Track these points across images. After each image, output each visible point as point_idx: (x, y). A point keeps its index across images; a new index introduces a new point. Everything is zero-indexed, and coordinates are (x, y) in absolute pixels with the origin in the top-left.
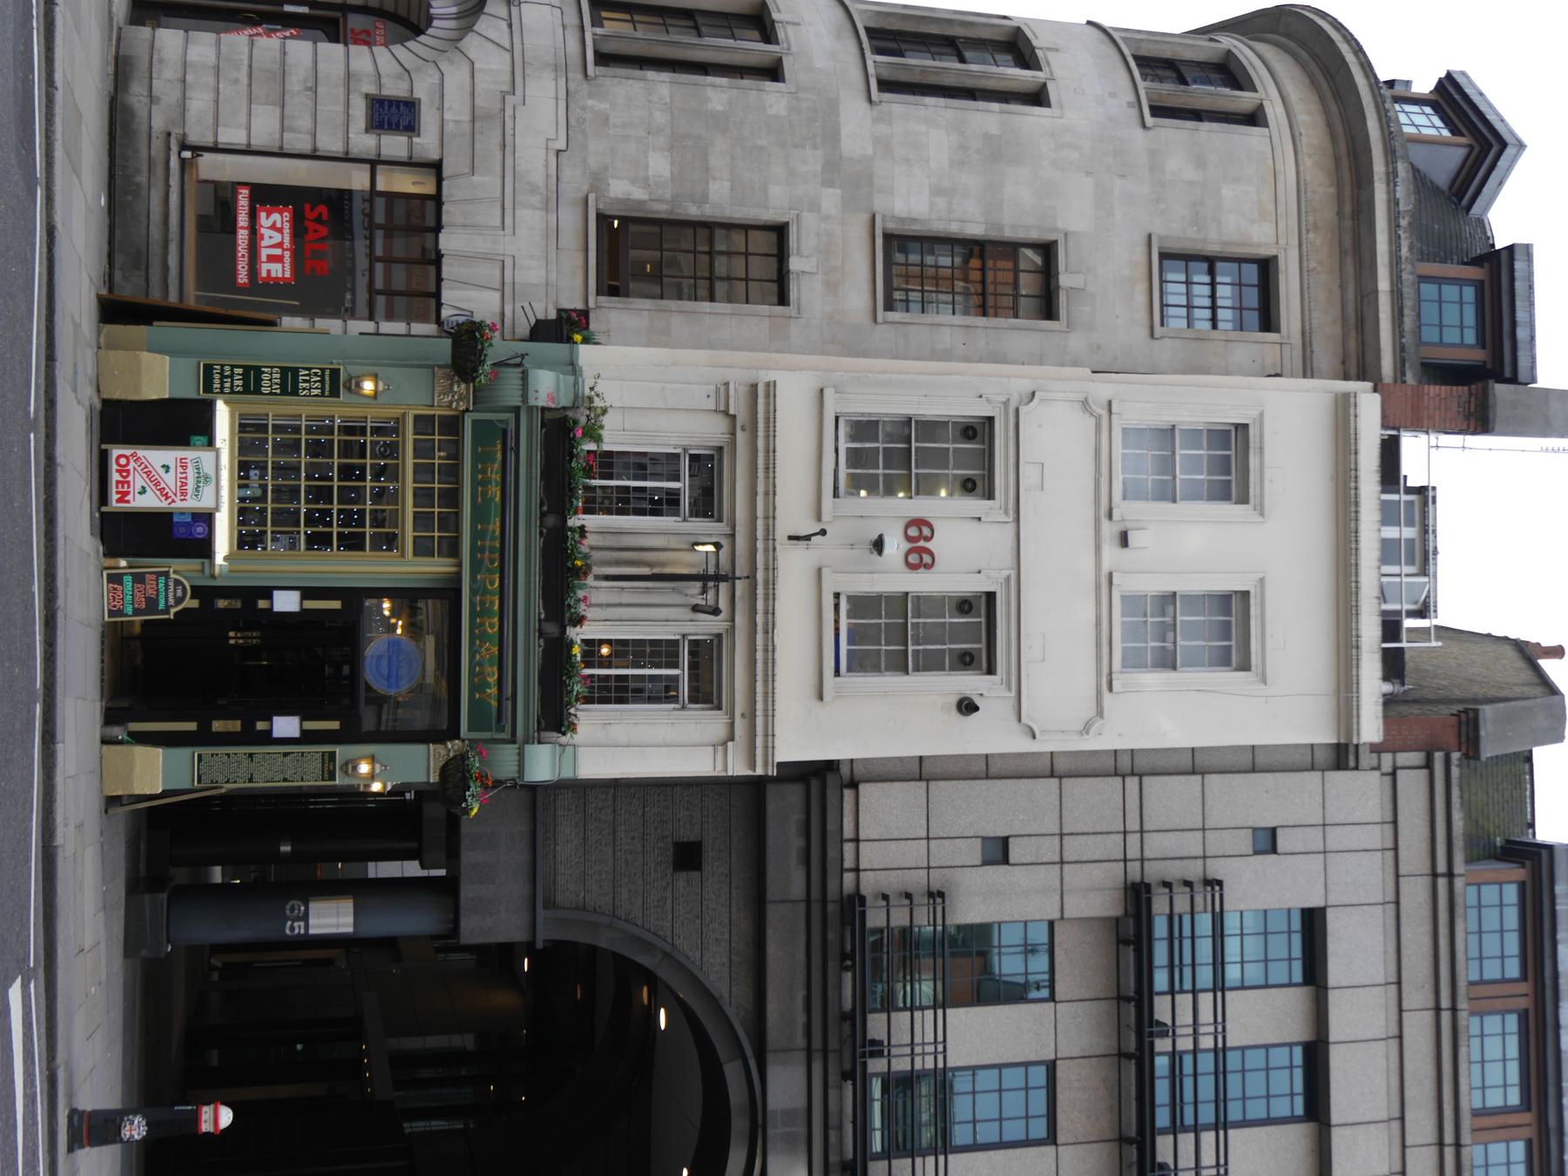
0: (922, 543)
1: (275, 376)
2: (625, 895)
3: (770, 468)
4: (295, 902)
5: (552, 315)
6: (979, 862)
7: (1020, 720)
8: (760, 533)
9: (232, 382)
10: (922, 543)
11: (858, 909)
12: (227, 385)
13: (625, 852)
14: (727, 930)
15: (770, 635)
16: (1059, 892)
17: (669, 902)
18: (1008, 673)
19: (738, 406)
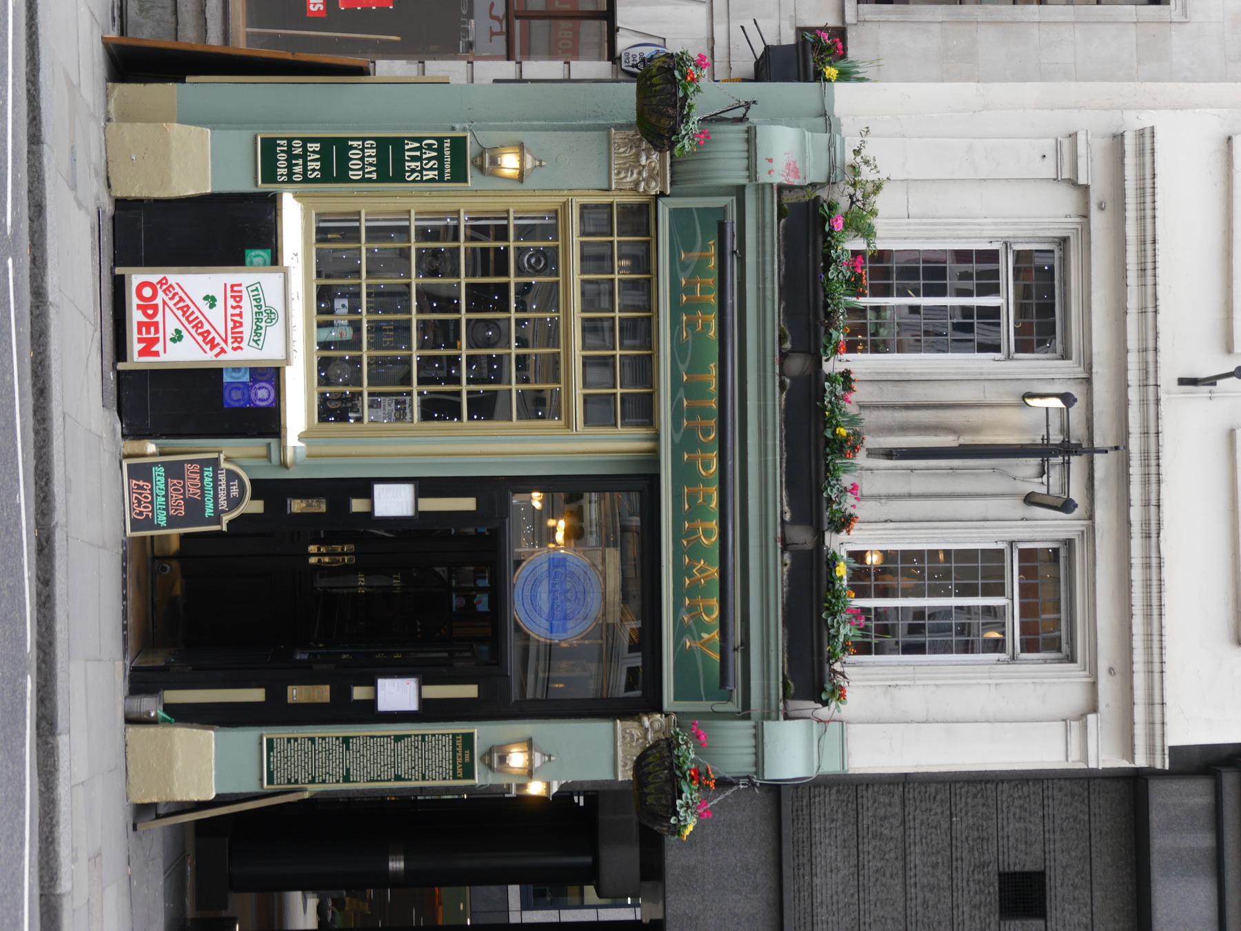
1: (368, 152)
12: (298, 169)
13: (923, 887)
19: (1093, 172)
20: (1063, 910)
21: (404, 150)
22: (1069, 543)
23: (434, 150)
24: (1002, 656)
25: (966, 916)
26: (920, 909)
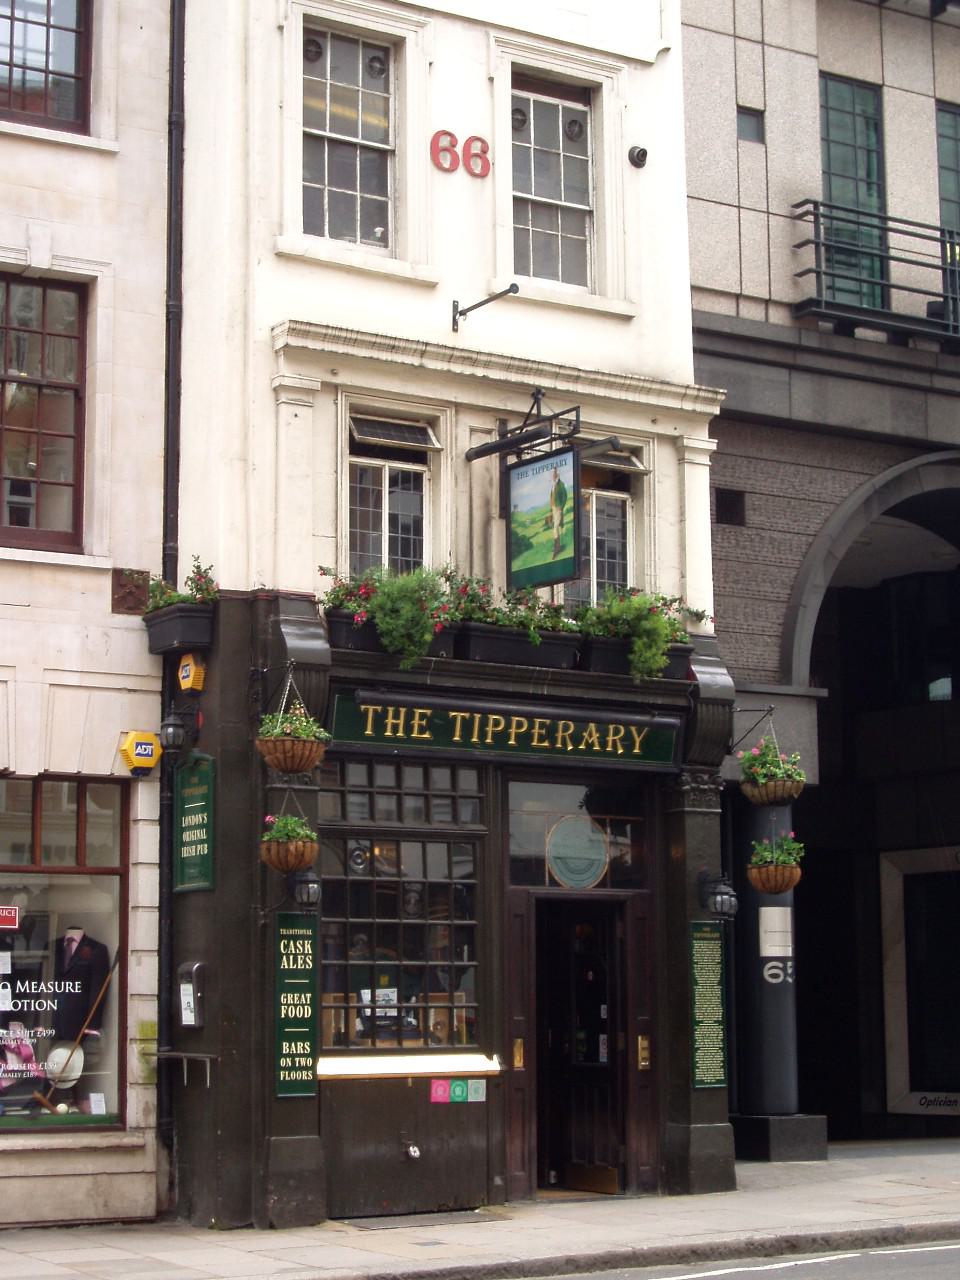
0: (459, 149)
1: (290, 1001)
2: (767, 587)
3: (393, 345)
4: (767, 973)
5: (781, 629)
6: (761, 148)
7: (647, 64)
8: (468, 370)
9: (300, 1055)
10: (459, 149)
11: (823, 310)
12: (303, 1061)
13: (726, 582)
14: (801, 468)
15: (582, 374)
16: (792, 54)
17: (775, 535)
18: (603, 67)
19: (313, 377)
20: (740, 478)
21: (289, 969)
22: (354, 409)
23: (289, 943)
24: (426, 476)
25: (743, 552)
26: (740, 586)
